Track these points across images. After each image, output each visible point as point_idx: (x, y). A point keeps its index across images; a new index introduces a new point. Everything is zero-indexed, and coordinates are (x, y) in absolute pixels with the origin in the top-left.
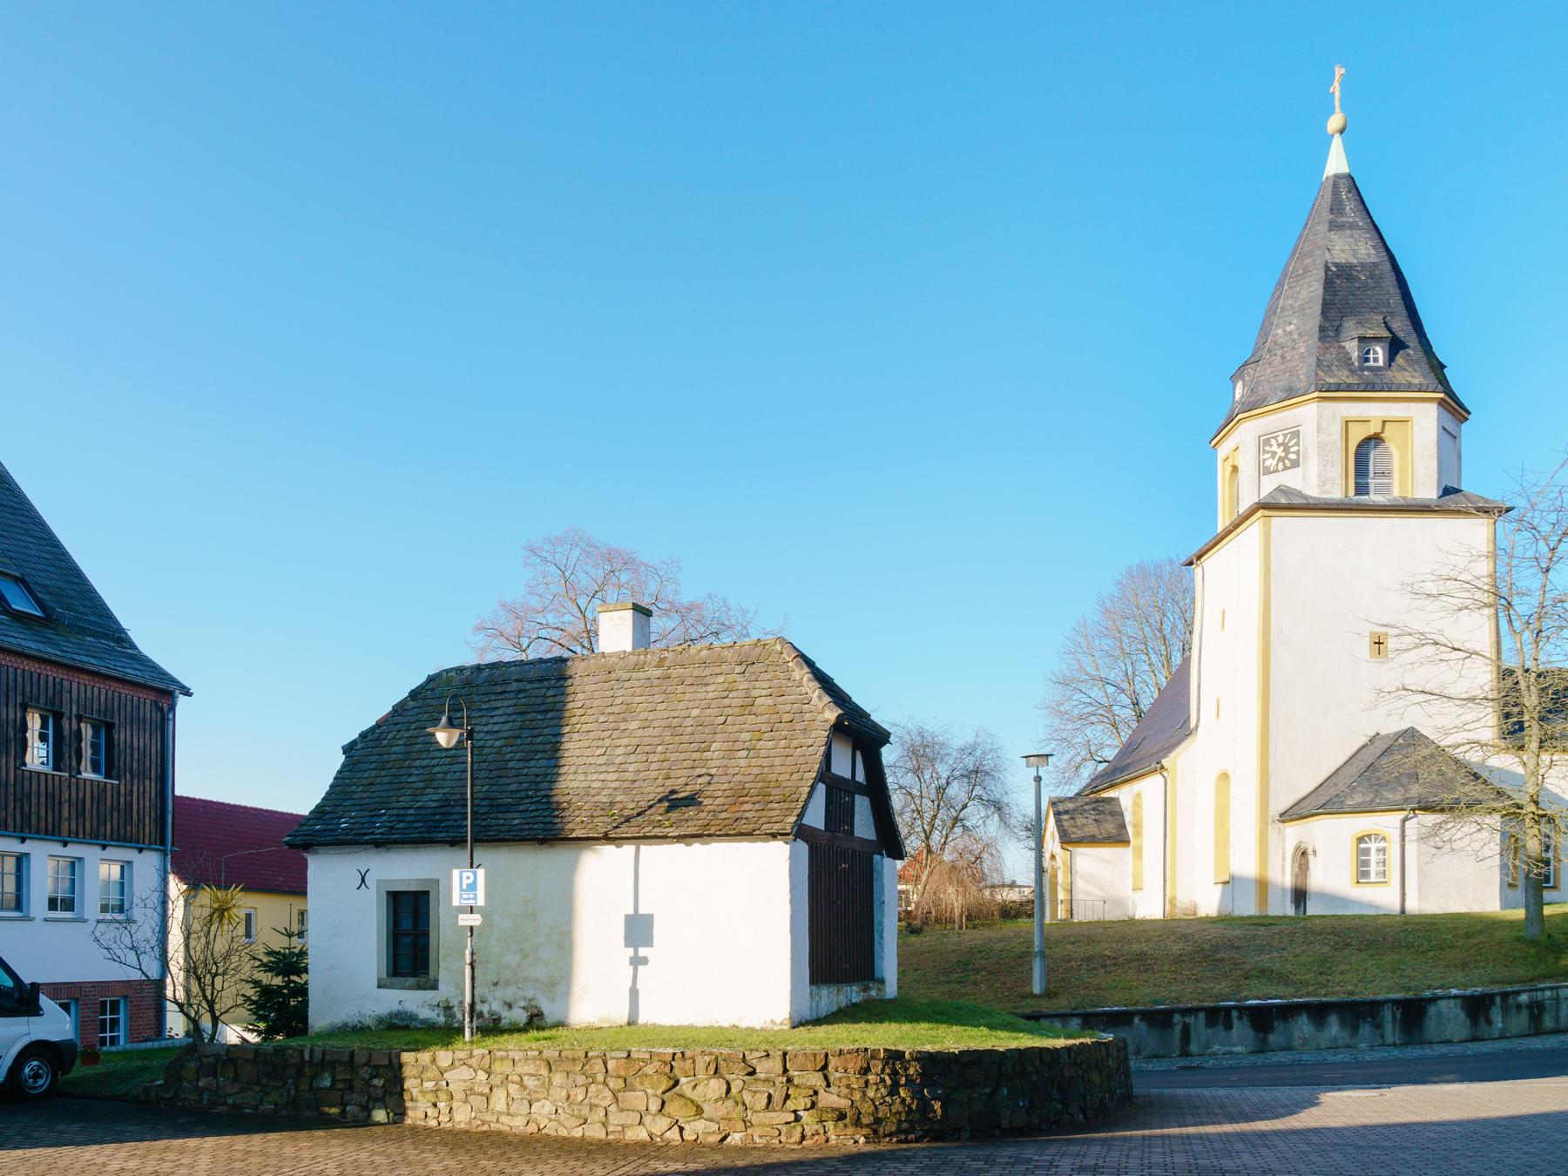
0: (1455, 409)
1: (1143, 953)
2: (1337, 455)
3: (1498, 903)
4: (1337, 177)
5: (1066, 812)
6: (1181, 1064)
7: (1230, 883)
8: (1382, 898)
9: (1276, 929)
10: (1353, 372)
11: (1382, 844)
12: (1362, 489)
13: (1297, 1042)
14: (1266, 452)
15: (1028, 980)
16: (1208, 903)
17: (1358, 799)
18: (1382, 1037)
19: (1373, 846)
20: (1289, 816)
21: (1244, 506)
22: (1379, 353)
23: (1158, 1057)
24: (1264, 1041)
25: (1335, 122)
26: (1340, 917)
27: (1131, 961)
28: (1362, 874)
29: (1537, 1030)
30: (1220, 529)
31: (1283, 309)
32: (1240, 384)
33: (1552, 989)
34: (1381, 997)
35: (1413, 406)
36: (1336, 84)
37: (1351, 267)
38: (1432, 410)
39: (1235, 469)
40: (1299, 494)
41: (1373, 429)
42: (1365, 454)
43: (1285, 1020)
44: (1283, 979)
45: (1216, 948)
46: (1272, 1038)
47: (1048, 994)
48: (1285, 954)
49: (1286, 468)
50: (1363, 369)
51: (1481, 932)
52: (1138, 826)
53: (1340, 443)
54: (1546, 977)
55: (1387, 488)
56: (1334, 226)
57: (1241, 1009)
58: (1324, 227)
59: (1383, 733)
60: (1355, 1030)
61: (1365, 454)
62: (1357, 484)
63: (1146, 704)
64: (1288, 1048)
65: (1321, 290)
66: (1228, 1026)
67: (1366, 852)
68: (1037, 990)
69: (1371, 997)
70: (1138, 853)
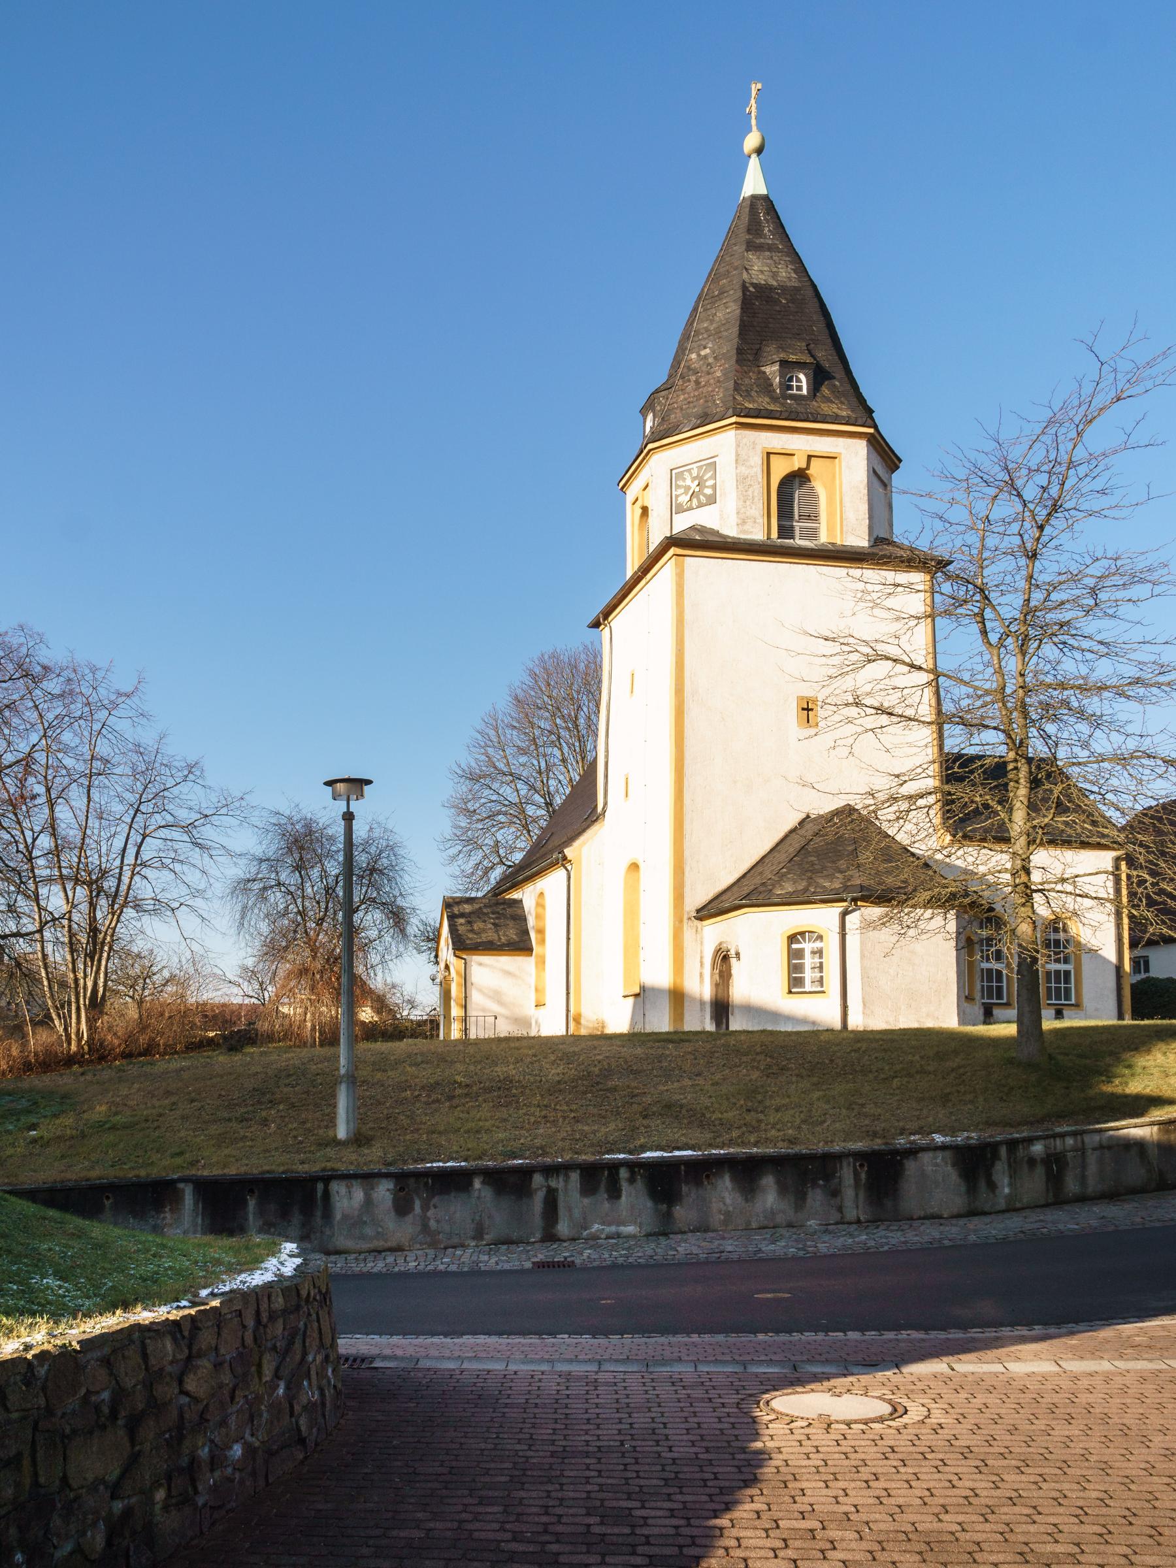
0: (885, 458)
1: (508, 1080)
2: (758, 490)
3: (956, 1018)
4: (754, 198)
5: (462, 915)
6: (540, 1257)
7: (642, 996)
8: (820, 1010)
9: (688, 1047)
10: (774, 399)
11: (818, 944)
12: (785, 531)
13: (717, 1219)
14: (678, 487)
15: (332, 1122)
16: (617, 1018)
17: (789, 887)
18: (840, 1209)
19: (807, 946)
20: (708, 911)
21: (656, 540)
22: (802, 382)
23: (509, 1242)
24: (667, 1217)
25: (752, 141)
26: (772, 1033)
27: (490, 1090)
28: (795, 983)
29: (1057, 1199)
30: (629, 574)
31: (697, 333)
32: (650, 417)
33: (1074, 1134)
34: (837, 1148)
35: (841, 441)
36: (753, 101)
37: (771, 288)
38: (860, 448)
39: (645, 510)
40: (717, 533)
41: (798, 463)
42: (791, 491)
43: (698, 1184)
44: (697, 1118)
45: (607, 1073)
46: (680, 1212)
47: (359, 1140)
48: (700, 1081)
49: (700, 505)
50: (785, 396)
51: (956, 1052)
52: (541, 931)
53: (761, 478)
54: (1061, 1116)
55: (813, 534)
56: (751, 246)
57: (631, 1166)
58: (740, 248)
59: (814, 813)
60: (800, 1199)
61: (791, 491)
62: (780, 527)
63: (558, 801)
64: (703, 1228)
65: (738, 311)
66: (614, 1193)
67: (799, 954)
68: (342, 1133)
69: (821, 1148)
70: (541, 962)
